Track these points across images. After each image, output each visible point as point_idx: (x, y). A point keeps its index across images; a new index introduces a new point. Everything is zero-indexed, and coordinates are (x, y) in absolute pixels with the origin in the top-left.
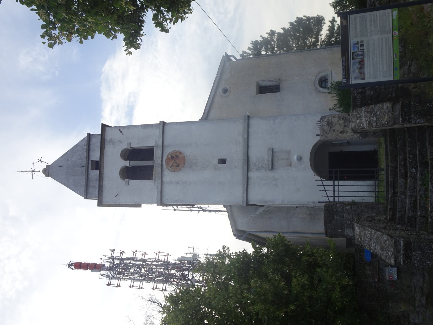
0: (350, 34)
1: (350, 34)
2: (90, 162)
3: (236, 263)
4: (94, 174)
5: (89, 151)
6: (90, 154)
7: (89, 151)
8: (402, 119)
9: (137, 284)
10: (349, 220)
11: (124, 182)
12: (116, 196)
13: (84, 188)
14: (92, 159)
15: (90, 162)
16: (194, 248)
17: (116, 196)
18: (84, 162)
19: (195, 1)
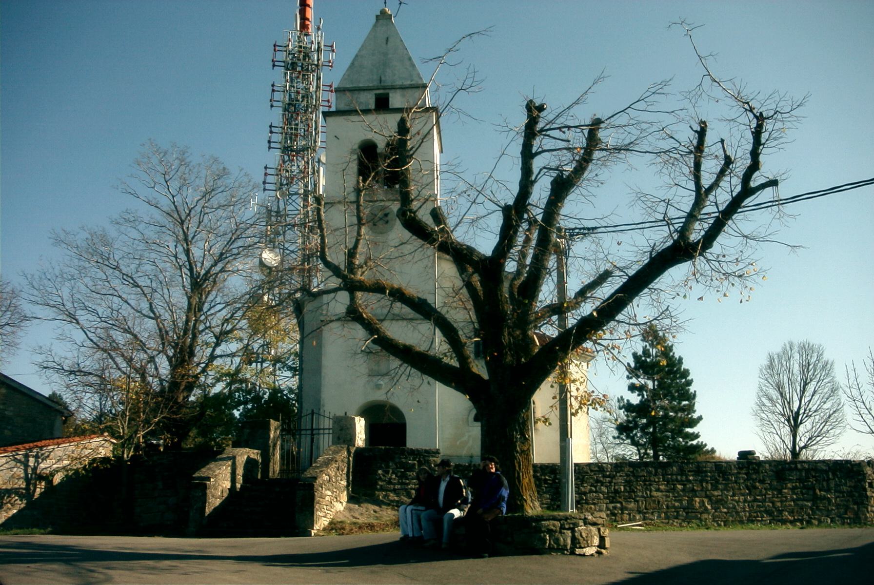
0: (129, 549)
1: (129, 549)
2: (387, 91)
3: (5, 516)
4: (369, 100)
5: (403, 88)
6: (398, 91)
7: (403, 88)
8: (530, 515)
9: (277, 138)
10: (675, 482)
11: (356, 147)
12: (336, 137)
13: (348, 85)
14: (391, 95)
15: (387, 91)
16: (480, 192)
17: (336, 137)
18: (389, 83)
19: (503, 204)
